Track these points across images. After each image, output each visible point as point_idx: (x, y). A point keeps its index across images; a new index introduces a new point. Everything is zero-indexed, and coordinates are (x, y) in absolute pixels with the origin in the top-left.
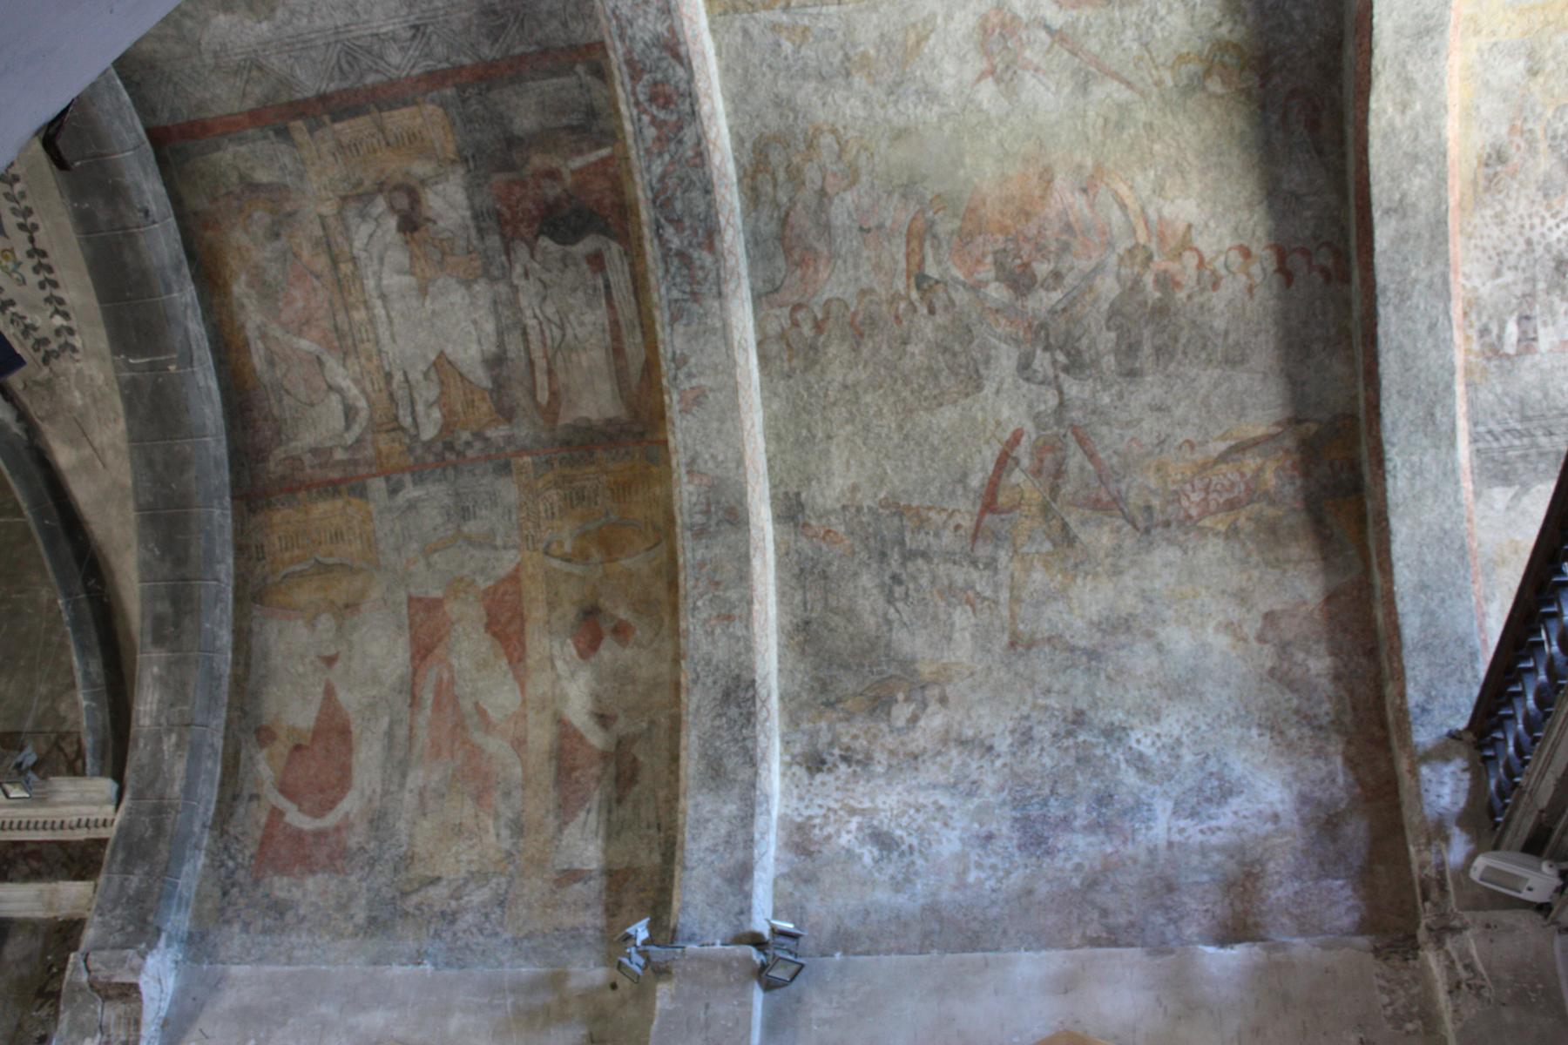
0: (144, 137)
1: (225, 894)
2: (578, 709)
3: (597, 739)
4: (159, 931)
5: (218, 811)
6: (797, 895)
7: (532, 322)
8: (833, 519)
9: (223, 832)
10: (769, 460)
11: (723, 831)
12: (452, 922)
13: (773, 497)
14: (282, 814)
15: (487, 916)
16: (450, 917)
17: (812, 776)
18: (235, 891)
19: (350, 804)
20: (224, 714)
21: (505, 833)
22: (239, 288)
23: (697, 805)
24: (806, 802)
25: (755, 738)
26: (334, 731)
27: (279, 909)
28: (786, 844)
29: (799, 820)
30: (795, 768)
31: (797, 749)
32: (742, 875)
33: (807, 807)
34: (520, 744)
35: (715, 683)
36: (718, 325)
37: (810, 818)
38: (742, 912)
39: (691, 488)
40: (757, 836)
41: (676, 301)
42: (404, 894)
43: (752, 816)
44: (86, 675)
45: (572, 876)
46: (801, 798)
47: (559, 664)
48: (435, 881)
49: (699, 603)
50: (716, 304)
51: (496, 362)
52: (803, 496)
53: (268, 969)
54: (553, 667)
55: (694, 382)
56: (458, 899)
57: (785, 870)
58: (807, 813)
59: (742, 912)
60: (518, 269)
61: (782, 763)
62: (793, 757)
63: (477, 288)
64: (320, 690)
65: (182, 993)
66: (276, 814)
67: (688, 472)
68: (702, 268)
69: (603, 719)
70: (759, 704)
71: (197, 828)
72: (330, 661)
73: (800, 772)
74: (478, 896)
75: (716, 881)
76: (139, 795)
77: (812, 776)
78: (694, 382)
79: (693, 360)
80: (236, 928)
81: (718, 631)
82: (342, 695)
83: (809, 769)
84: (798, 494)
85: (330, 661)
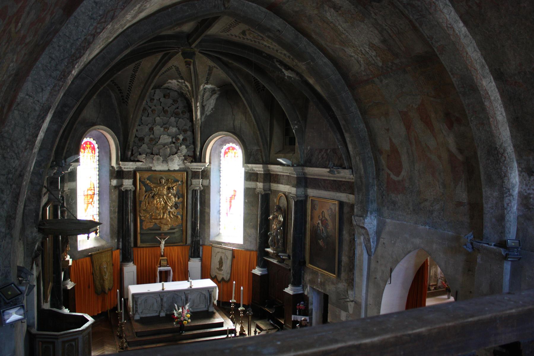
0: (267, 11)
1: (382, 198)
2: (453, 148)
3: (460, 157)
4: (367, 211)
5: (376, 173)
6: (525, 224)
7: (387, 27)
8: (516, 77)
9: (379, 180)
10: (484, 58)
11: (494, 202)
12: (432, 214)
13: (491, 71)
14: (390, 175)
15: (440, 213)
16: (431, 212)
17: (530, 177)
18: (384, 197)
19: (403, 173)
20: (370, 146)
21: (441, 187)
22: (314, 36)
23: (486, 191)
24: (528, 187)
25: (501, 169)
26: (394, 150)
27: (394, 203)
28: (521, 204)
29: (525, 194)
30: (523, 173)
31: (523, 166)
32: (501, 219)
33: (529, 189)
34: (439, 157)
35: (484, 147)
36: (436, 23)
37: (529, 194)
38: (502, 233)
39: (455, 79)
40: (505, 205)
41: (417, 19)
42: (420, 203)
43: (503, 198)
44: (337, 139)
45: (460, 204)
46: (526, 185)
47: (444, 131)
48: (426, 200)
49: (472, 119)
50: (431, 17)
51: (384, 41)
52: (502, 69)
53: (394, 221)
54: (442, 133)
55: (439, 44)
56: (432, 207)
57: (521, 214)
58: (528, 192)
59: (502, 233)
60: (373, 15)
61: (518, 171)
62: (522, 169)
63: (366, 22)
64: (388, 139)
65: (378, 225)
66: (389, 175)
67: (452, 74)
68: (419, 6)
69: (461, 151)
70: (500, 156)
71: (371, 181)
72: (388, 130)
73: (525, 175)
74: (437, 207)
75: (494, 220)
76: (356, 173)
77: (530, 177)
78: (439, 44)
79: (434, 37)
80: (386, 208)
81: (481, 129)
82: (393, 140)
83: (528, 174)
84: (500, 69)
85: (388, 130)
